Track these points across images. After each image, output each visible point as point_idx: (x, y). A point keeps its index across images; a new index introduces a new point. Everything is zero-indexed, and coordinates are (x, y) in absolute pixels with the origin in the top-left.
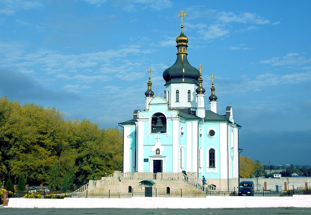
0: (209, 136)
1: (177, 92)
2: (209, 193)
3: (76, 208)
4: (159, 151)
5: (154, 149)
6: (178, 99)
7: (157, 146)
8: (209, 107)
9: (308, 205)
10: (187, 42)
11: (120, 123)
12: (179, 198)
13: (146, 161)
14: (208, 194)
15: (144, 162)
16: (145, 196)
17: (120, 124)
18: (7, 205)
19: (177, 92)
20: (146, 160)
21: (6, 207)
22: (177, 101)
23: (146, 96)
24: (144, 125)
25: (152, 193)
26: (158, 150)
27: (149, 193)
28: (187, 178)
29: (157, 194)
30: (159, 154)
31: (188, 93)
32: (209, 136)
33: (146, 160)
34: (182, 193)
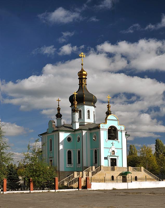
1: (89, 111)
5: (111, 151)
7: (113, 149)
8: (90, 124)
10: (86, 76)
11: (40, 135)
12: (103, 183)
13: (106, 158)
14: (105, 181)
15: (105, 159)
16: (123, 182)
17: (39, 136)
18: (90, 188)
19: (89, 111)
20: (106, 158)
21: (90, 189)
22: (89, 118)
24: (104, 135)
26: (113, 151)
27: (125, 180)
28: (144, 171)
29: (92, 180)
30: (114, 154)
31: (88, 112)
33: (106, 158)
34: (105, 179)
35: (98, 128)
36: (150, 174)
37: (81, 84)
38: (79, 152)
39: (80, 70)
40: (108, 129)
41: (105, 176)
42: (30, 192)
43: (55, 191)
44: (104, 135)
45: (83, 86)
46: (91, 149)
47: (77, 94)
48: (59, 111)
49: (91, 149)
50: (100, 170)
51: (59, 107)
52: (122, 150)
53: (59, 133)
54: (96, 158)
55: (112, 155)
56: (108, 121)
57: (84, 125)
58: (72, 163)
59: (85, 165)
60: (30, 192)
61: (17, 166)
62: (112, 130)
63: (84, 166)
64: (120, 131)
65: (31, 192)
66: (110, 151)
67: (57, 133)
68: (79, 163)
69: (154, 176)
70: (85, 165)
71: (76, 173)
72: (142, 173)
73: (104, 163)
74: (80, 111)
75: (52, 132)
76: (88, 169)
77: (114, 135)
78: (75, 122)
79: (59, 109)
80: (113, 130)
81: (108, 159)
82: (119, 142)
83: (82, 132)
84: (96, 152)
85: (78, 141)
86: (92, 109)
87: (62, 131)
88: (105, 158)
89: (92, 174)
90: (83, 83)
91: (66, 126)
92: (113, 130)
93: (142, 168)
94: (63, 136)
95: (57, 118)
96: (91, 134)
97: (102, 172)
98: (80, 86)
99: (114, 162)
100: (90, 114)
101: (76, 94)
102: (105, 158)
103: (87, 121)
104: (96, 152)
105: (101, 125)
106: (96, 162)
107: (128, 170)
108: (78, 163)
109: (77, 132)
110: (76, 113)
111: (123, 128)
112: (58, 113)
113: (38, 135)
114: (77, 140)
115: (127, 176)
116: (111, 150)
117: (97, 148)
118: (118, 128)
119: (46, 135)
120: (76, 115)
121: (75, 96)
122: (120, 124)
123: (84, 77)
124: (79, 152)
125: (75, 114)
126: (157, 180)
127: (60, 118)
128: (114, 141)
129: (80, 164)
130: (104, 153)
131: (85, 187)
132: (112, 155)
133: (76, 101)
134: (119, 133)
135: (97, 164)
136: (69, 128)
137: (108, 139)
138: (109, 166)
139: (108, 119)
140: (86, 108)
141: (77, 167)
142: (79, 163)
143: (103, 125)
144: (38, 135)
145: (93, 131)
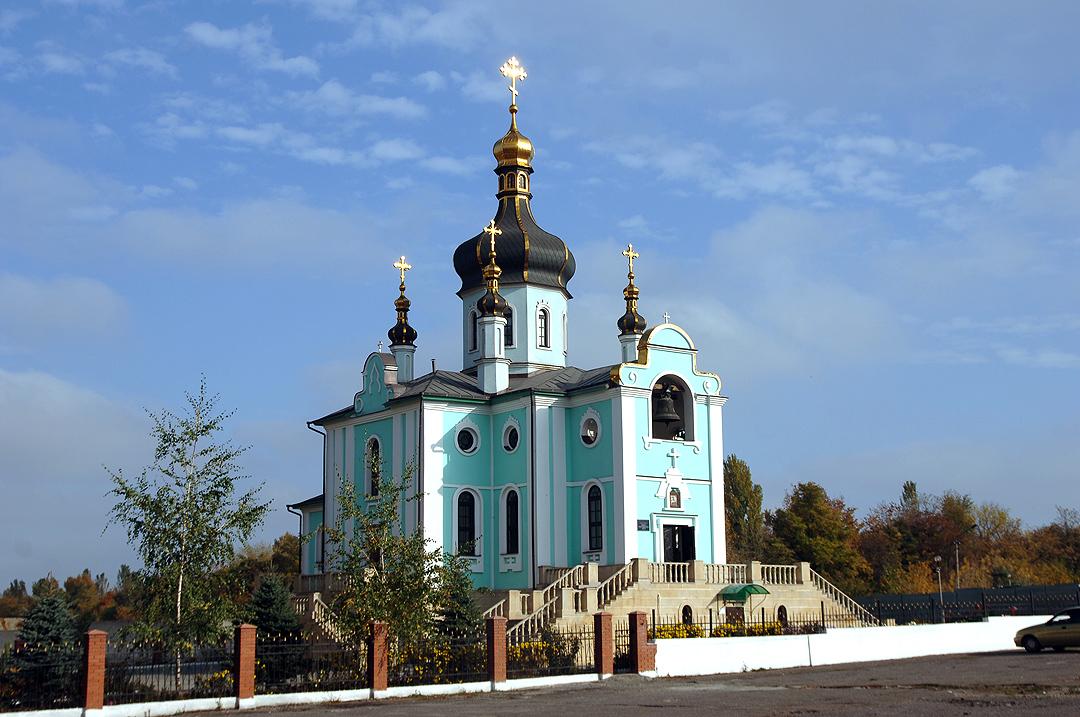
1: (545, 315)
4: (675, 499)
5: (664, 490)
15: (639, 529)
18: (652, 668)
20: (643, 525)
21: (651, 674)
24: (635, 413)
26: (676, 493)
27: (735, 626)
33: (643, 525)
35: (607, 381)
36: (836, 594)
37: (507, 194)
38: (512, 501)
39: (504, 132)
40: (652, 388)
41: (655, 608)
42: (372, 695)
43: (600, 678)
44: (635, 413)
45: (517, 200)
46: (570, 484)
47: (500, 232)
48: (405, 315)
49: (570, 484)
50: (635, 579)
51: (402, 297)
52: (710, 486)
53: (421, 410)
54: (595, 525)
55: (669, 508)
56: (651, 353)
57: (525, 376)
58: (477, 553)
59: (543, 560)
60: (372, 695)
61: (113, 584)
62: (666, 394)
63: (539, 563)
64: (704, 398)
65: (379, 694)
66: (662, 494)
67: (410, 411)
68: (513, 547)
69: (861, 611)
70: (543, 560)
71: (515, 599)
72: (805, 595)
73: (641, 547)
74: (508, 315)
75: (386, 405)
76: (618, 576)
77: (678, 418)
78: (494, 360)
79: (403, 306)
80: (674, 395)
81: (655, 529)
82: (696, 450)
83: (533, 404)
84: (595, 496)
85: (507, 448)
86: (555, 300)
87: (437, 398)
88: (640, 523)
89: (599, 603)
90: (519, 189)
91: (459, 383)
92: (674, 395)
93: (806, 567)
94: (440, 421)
95: (396, 347)
96: (569, 411)
97: (644, 590)
98: (501, 203)
99: (680, 545)
100: (548, 329)
101: (497, 235)
102: (640, 523)
103: (536, 356)
104: (595, 496)
105: (623, 372)
106: (596, 544)
107: (749, 580)
108: (506, 552)
109: (502, 408)
110: (497, 318)
111: (713, 388)
112: (400, 322)
113: (309, 423)
114: (504, 441)
115: (746, 607)
116: (664, 485)
117: (603, 480)
118: (694, 384)
119: (350, 427)
120: (496, 326)
121: (493, 242)
122: (701, 369)
123: (521, 162)
124: (512, 501)
125: (493, 322)
126: (867, 620)
127: (407, 344)
128: (676, 445)
129: (518, 557)
130: (638, 500)
131: (628, 663)
132: (669, 508)
133: (498, 264)
134: (699, 409)
135: (604, 554)
136: (465, 385)
137: (653, 437)
138: (658, 562)
139: (650, 341)
140: (536, 297)
141: (503, 568)
142: (513, 547)
143: (633, 371)
144: (309, 423)
145: (579, 401)
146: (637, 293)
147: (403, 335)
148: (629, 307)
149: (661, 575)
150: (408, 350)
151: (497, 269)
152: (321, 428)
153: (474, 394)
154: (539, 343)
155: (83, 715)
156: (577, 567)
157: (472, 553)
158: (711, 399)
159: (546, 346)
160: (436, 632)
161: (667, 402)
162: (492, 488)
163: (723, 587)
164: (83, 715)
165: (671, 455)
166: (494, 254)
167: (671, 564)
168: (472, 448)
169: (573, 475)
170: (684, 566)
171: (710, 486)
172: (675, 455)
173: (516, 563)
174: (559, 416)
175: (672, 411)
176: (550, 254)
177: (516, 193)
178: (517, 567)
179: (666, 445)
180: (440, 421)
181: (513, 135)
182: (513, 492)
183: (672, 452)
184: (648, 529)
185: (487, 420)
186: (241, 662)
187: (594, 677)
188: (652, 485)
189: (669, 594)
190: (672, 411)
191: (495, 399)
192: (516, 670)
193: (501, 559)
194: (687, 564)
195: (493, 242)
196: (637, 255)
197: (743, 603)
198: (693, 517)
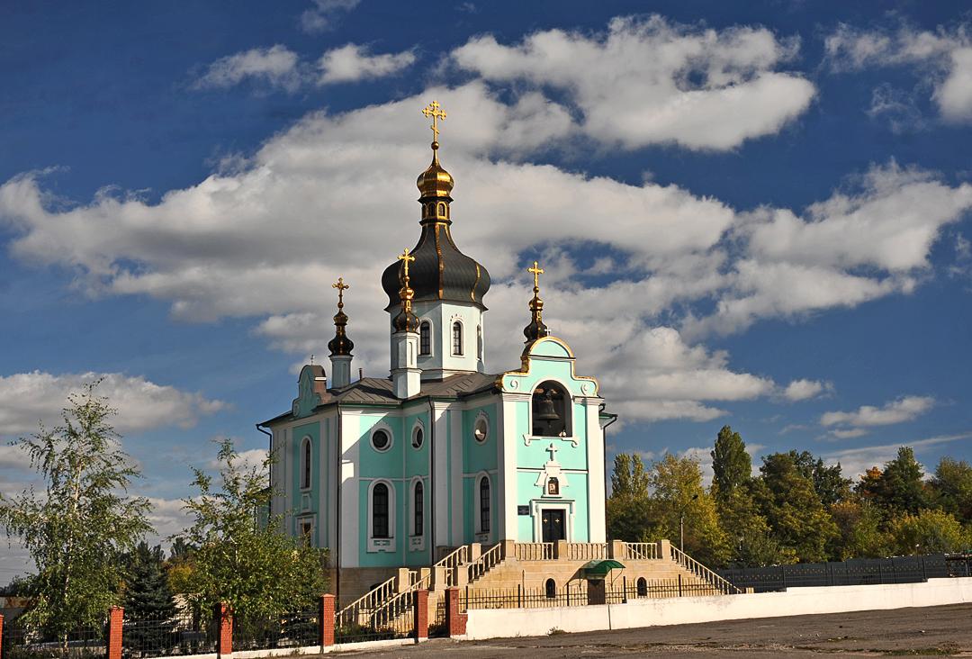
0: (389, 446)
1: (458, 327)
2: (524, 601)
3: (720, 622)
4: (554, 486)
5: (543, 479)
6: (426, 346)
9: (964, 597)
12: (675, 599)
15: (519, 514)
18: (464, 632)
19: (458, 327)
20: (524, 510)
22: (459, 352)
23: (397, 328)
24: (516, 416)
25: (605, 593)
26: (554, 481)
27: (597, 596)
30: (558, 493)
32: (389, 446)
33: (524, 510)
34: (521, 594)
35: (493, 389)
39: (426, 167)
44: (516, 416)
45: (437, 226)
46: (466, 475)
47: (413, 259)
49: (466, 475)
50: (503, 558)
51: (341, 313)
52: (587, 475)
53: (340, 417)
56: (532, 363)
58: (390, 535)
59: (441, 539)
64: (581, 399)
66: (541, 482)
67: (331, 414)
68: (419, 532)
70: (441, 539)
71: (404, 574)
72: (666, 566)
73: (519, 530)
74: (425, 328)
75: (313, 410)
80: (553, 397)
81: (534, 513)
83: (433, 409)
85: (415, 446)
87: (354, 406)
88: (520, 508)
90: (439, 217)
94: (356, 426)
95: (334, 357)
101: (410, 262)
102: (520, 508)
103: (450, 363)
104: (484, 486)
105: (506, 381)
108: (414, 533)
109: (413, 411)
111: (591, 390)
113: (258, 425)
114: (412, 439)
116: (543, 476)
118: (573, 388)
119: (289, 426)
120: (408, 340)
121: (406, 268)
122: (578, 374)
125: (405, 338)
127: (344, 354)
129: (422, 538)
130: (518, 488)
134: (577, 410)
135: (490, 535)
136: (381, 394)
137: (533, 435)
138: (537, 542)
141: (412, 548)
144: (258, 425)
145: (474, 404)
146: (541, 305)
147: (341, 347)
148: (534, 317)
149: (538, 552)
150: (344, 360)
151: (409, 291)
152: (267, 430)
153: (388, 400)
154: (453, 353)
155: (219, 657)
156: (462, 547)
157: (386, 536)
158: (588, 400)
159: (460, 354)
160: (234, 609)
161: (547, 405)
162: (404, 479)
163: (585, 562)
164: (219, 657)
165: (550, 449)
166: (408, 278)
167: (547, 544)
168: (387, 444)
169: (468, 468)
170: (550, 545)
171: (587, 475)
172: (553, 449)
173: (422, 543)
174: (457, 416)
175: (551, 412)
176: (463, 272)
177: (437, 220)
178: (421, 547)
179: (545, 442)
180: (356, 426)
181: (436, 168)
182: (419, 483)
183: (551, 446)
184: (528, 514)
185: (399, 423)
186: (112, 635)
187: (412, 641)
188: (533, 476)
189: (532, 570)
190: (551, 412)
191: (407, 402)
192: (340, 639)
193: (411, 540)
194: (552, 544)
195: (406, 268)
196: (542, 271)
197: (604, 576)
198: (570, 502)
